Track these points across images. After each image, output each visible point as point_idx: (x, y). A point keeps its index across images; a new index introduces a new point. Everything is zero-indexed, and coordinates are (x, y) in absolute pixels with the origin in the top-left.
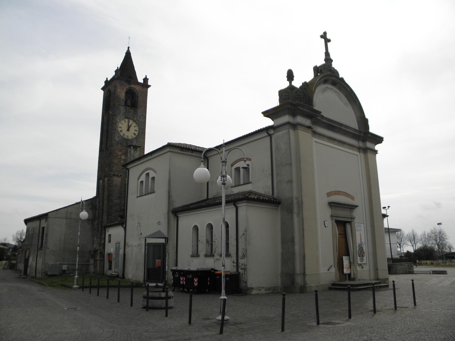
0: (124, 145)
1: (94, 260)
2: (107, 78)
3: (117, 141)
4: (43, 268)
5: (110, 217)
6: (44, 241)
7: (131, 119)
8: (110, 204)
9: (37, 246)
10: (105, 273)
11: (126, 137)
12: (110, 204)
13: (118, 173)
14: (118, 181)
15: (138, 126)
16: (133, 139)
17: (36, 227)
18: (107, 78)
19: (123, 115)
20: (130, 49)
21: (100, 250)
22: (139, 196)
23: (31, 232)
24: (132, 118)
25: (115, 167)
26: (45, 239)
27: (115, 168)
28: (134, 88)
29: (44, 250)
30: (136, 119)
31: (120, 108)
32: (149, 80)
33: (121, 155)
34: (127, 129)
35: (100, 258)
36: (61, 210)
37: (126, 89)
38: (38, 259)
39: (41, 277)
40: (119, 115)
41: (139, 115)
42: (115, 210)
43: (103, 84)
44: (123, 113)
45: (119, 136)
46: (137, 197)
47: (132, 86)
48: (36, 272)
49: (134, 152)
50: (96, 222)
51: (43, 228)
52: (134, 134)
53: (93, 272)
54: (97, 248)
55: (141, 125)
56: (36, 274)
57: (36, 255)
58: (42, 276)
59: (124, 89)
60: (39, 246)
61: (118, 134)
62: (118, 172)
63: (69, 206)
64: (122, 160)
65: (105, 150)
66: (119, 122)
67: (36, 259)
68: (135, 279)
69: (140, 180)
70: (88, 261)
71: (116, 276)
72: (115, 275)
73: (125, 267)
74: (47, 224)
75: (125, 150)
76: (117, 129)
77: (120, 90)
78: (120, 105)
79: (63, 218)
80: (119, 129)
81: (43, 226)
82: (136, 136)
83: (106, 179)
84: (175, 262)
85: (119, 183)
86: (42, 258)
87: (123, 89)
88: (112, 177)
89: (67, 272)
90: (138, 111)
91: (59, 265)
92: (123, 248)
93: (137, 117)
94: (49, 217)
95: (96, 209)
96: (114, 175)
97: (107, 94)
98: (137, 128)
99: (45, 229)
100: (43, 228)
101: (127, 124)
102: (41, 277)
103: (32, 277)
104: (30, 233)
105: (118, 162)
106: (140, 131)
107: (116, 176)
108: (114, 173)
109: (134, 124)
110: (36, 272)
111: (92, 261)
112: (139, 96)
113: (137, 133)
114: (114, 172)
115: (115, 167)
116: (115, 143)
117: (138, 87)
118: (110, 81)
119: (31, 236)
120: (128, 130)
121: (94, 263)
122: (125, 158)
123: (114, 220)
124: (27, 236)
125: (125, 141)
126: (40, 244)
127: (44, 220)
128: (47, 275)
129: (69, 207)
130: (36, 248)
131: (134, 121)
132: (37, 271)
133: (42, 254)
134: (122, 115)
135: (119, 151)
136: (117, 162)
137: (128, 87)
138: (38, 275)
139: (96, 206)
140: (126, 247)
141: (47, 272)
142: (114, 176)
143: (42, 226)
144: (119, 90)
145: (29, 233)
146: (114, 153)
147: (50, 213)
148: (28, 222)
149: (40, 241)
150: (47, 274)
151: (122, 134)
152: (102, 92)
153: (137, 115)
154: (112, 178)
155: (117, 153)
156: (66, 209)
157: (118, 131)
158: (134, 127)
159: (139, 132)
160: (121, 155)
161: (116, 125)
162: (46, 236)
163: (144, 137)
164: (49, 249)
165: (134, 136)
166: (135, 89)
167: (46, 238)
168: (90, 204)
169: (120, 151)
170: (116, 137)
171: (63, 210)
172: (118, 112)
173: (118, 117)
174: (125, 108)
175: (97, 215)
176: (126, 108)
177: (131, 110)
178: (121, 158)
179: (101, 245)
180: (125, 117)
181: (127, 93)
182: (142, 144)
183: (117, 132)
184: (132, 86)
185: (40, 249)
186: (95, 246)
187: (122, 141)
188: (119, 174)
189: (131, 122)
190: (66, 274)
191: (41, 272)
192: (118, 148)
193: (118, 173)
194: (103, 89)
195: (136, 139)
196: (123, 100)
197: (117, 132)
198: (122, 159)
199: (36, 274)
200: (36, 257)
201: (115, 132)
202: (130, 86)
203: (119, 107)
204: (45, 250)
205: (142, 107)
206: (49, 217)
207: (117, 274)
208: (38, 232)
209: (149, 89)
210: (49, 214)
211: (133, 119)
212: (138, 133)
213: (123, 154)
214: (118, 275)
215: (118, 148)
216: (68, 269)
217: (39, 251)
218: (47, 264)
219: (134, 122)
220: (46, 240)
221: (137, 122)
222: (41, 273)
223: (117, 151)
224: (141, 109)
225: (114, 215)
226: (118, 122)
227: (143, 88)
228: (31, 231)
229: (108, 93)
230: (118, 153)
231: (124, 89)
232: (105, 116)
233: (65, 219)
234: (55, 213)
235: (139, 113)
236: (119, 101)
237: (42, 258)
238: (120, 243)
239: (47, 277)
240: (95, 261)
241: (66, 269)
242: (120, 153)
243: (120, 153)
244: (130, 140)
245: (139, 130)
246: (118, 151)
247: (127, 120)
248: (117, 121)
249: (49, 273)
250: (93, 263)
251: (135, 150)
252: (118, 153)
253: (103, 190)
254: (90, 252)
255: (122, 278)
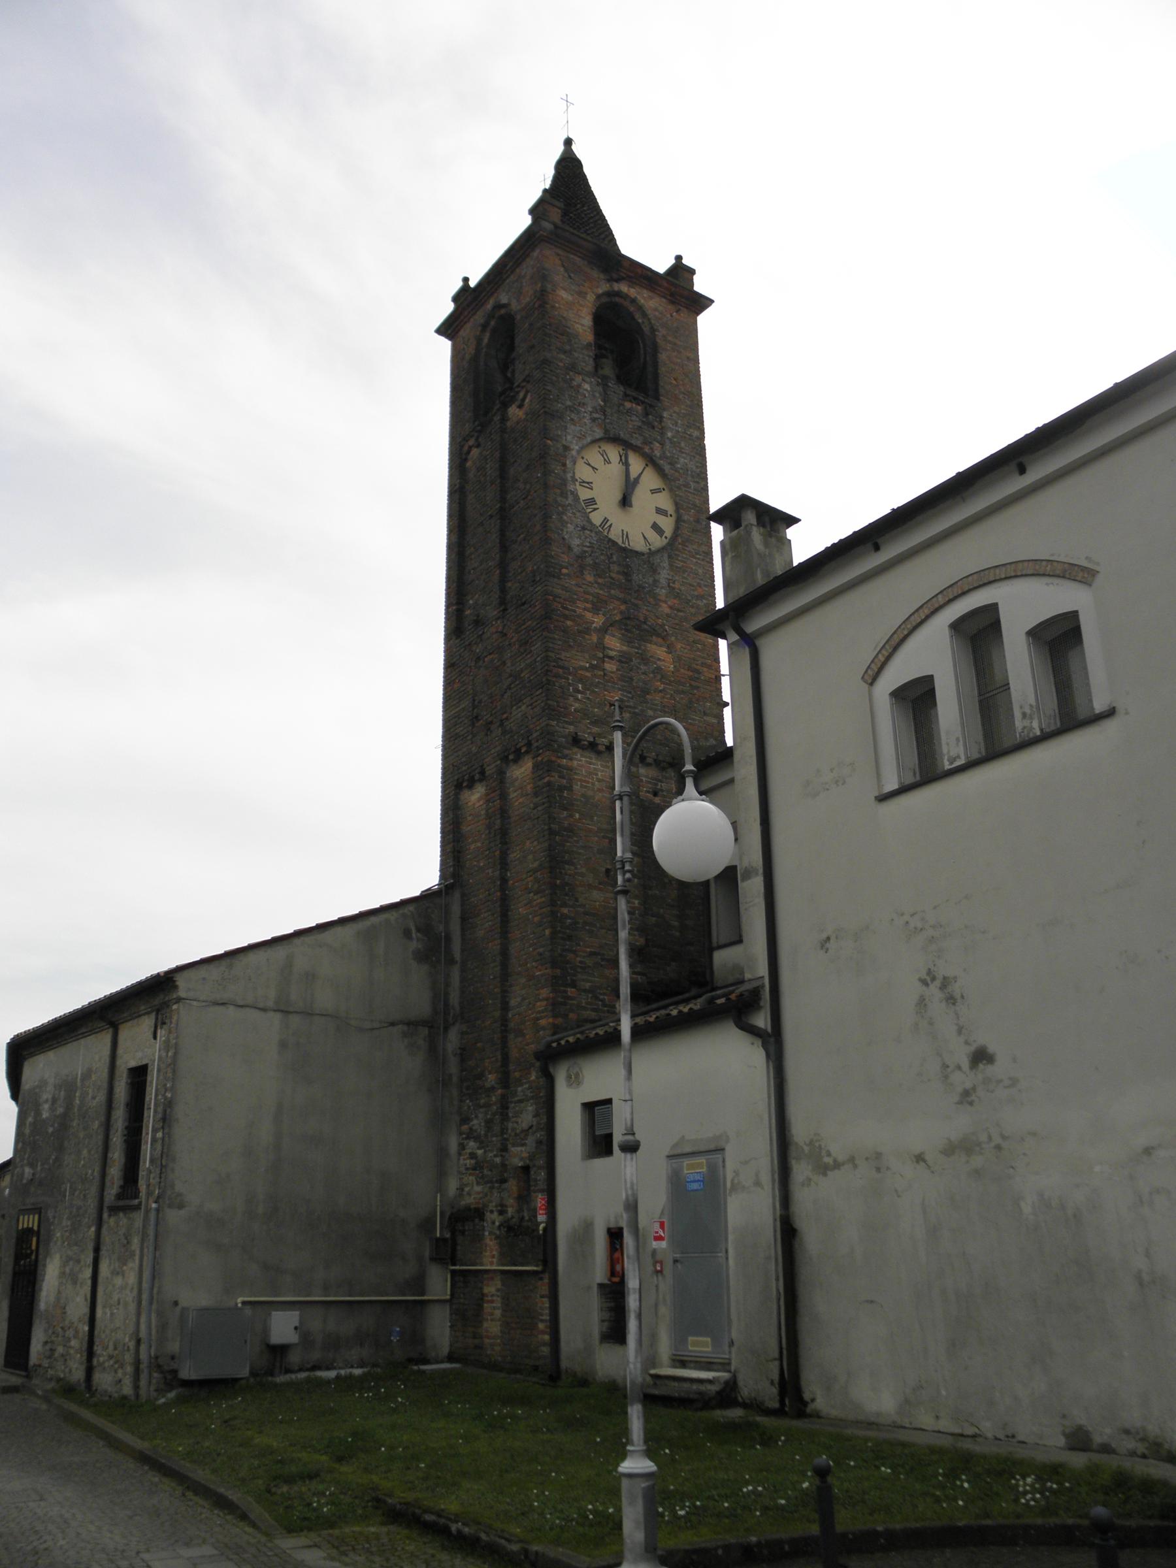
0: (614, 575)
1: (454, 1273)
2: (466, 280)
3: (576, 550)
4: (143, 1334)
5: (571, 991)
6: (147, 1150)
7: (636, 449)
8: (565, 911)
9: (93, 1190)
10: (564, 1363)
11: (615, 535)
12: (565, 911)
13: (595, 730)
14: (599, 780)
15: (671, 490)
16: (652, 553)
17: (87, 1075)
18: (466, 280)
19: (594, 420)
20: (574, 147)
21: (501, 1213)
22: (892, 785)
23: (52, 1109)
24: (639, 443)
25: (580, 696)
26: (154, 1140)
27: (577, 699)
28: (633, 301)
29: (152, 1215)
30: (657, 453)
31: (575, 383)
32: (695, 277)
33: (603, 630)
34: (618, 496)
35: (505, 1257)
36: (252, 957)
37: (599, 297)
38: (104, 1269)
39: (127, 1389)
40: (573, 415)
41: (669, 434)
42: (592, 954)
43: (448, 308)
44: (595, 410)
45: (584, 528)
46: (883, 798)
47: (624, 288)
48: (90, 1353)
49: (766, 545)
50: (453, 1040)
51: (139, 1074)
52: (655, 527)
53: (445, 1350)
54: (469, 1200)
55: (687, 485)
56: (89, 1371)
57: (91, 1246)
58: (136, 1387)
59: (586, 294)
60: (112, 1191)
61: (578, 514)
62: (595, 723)
63: (299, 934)
64: (611, 658)
65: (492, 612)
66: (579, 452)
67: (88, 1273)
68: (946, 1425)
69: (898, 673)
70: (418, 1283)
71: (719, 1393)
72: (714, 1388)
73: (805, 1323)
74: (167, 1046)
75: (623, 607)
76: (571, 487)
77: (570, 298)
78: (572, 367)
79: (264, 1010)
80: (584, 494)
81: (133, 1064)
82: (665, 542)
83: (522, 772)
84: (776, 1286)
85: (600, 790)
86: (134, 1264)
87: (582, 294)
88: (566, 752)
89: (294, 1358)
90: (665, 414)
91: (248, 1311)
92: (757, 1183)
93: (662, 444)
94: (179, 1000)
95: (451, 961)
96: (576, 741)
97: (479, 340)
98: (664, 501)
99: (153, 1080)
100: (139, 1074)
101: (615, 468)
102: (127, 1389)
103: (68, 1390)
104: (45, 1115)
105: (593, 667)
106: (686, 517)
107: (583, 748)
108: (572, 728)
109: (650, 480)
110: (90, 1353)
111: (439, 1284)
112: (658, 341)
113: (667, 524)
114: (570, 723)
115: (580, 696)
116: (565, 559)
117: (651, 298)
118: (505, 266)
119: (50, 1130)
120: (625, 502)
121: (452, 1295)
122: (625, 648)
123: (593, 1015)
124: (27, 1131)
125: (615, 558)
126: (115, 1172)
127: (147, 1023)
128: (171, 1379)
129: (297, 941)
130: (92, 1204)
131: (651, 461)
132: (98, 1349)
133: (136, 1241)
134: (587, 421)
135: (589, 606)
136: (582, 664)
137: (603, 288)
138: (103, 1380)
139: (448, 938)
140: (800, 1171)
141: (173, 1358)
142: (575, 750)
143: (129, 1059)
144: (563, 294)
145: (38, 1113)
146: (566, 617)
147: (186, 973)
148: (32, 1055)
149: (117, 1155)
150: (175, 1372)
151: (596, 518)
152: (445, 346)
153: (662, 434)
154: (565, 757)
155: (581, 616)
156: (280, 952)
157: (576, 498)
158: (653, 491)
159: (679, 520)
160: (603, 630)
161: (564, 465)
162: (166, 1120)
163: (704, 548)
164: (181, 1206)
165: (657, 542)
166: (640, 308)
167: (159, 1135)
168: (418, 930)
169: (596, 609)
170: (570, 527)
171: (261, 955)
172: (569, 403)
173: (572, 428)
174: (600, 389)
175: (455, 999)
176: (605, 391)
177: (628, 405)
178: (601, 646)
179: (503, 1181)
180: (606, 431)
181: (599, 319)
182: (699, 585)
183: (570, 500)
184: (624, 288)
185: (114, 1210)
186: (452, 1185)
187: (602, 557)
188: (600, 735)
189: (636, 464)
190: (288, 1371)
191: (128, 1358)
192: (588, 593)
193: (595, 730)
194: (447, 329)
195: (670, 557)
196: (589, 345)
197: (570, 505)
198: (612, 653)
199: (89, 1371)
200: (89, 1258)
201: (559, 499)
202: (616, 287)
203: (572, 380)
204: (158, 1210)
205: (681, 396)
206: (179, 1000)
207: (724, 1375)
208: (101, 1097)
209: (704, 320)
210: (181, 981)
211: (647, 450)
212: (677, 528)
213: (611, 625)
214: (731, 1386)
215: (588, 593)
216: (306, 1338)
217: (110, 1221)
218: (176, 1303)
219: (647, 468)
220: (159, 1146)
221: (667, 468)
222: (129, 1369)
223: (579, 604)
224: (676, 409)
225: (587, 985)
226: (574, 453)
227: (677, 311)
228: (54, 1100)
229: (487, 335)
230: (589, 615)
231: (588, 297)
232: (475, 452)
233: (276, 1018)
234: (214, 972)
235: (669, 424)
236: (567, 347)
237: (134, 1264)
238: (721, 1150)
239: (172, 1395)
240: (462, 1280)
241: (292, 1338)
242: (598, 621)
243: (598, 621)
244: (643, 554)
245: (677, 510)
246: (585, 609)
247: (613, 452)
248: (567, 448)
249: (187, 1372)
250: (448, 1297)
251: (771, 536)
252: (589, 615)
253: (502, 835)
254: (426, 1224)
255: (779, 1412)
